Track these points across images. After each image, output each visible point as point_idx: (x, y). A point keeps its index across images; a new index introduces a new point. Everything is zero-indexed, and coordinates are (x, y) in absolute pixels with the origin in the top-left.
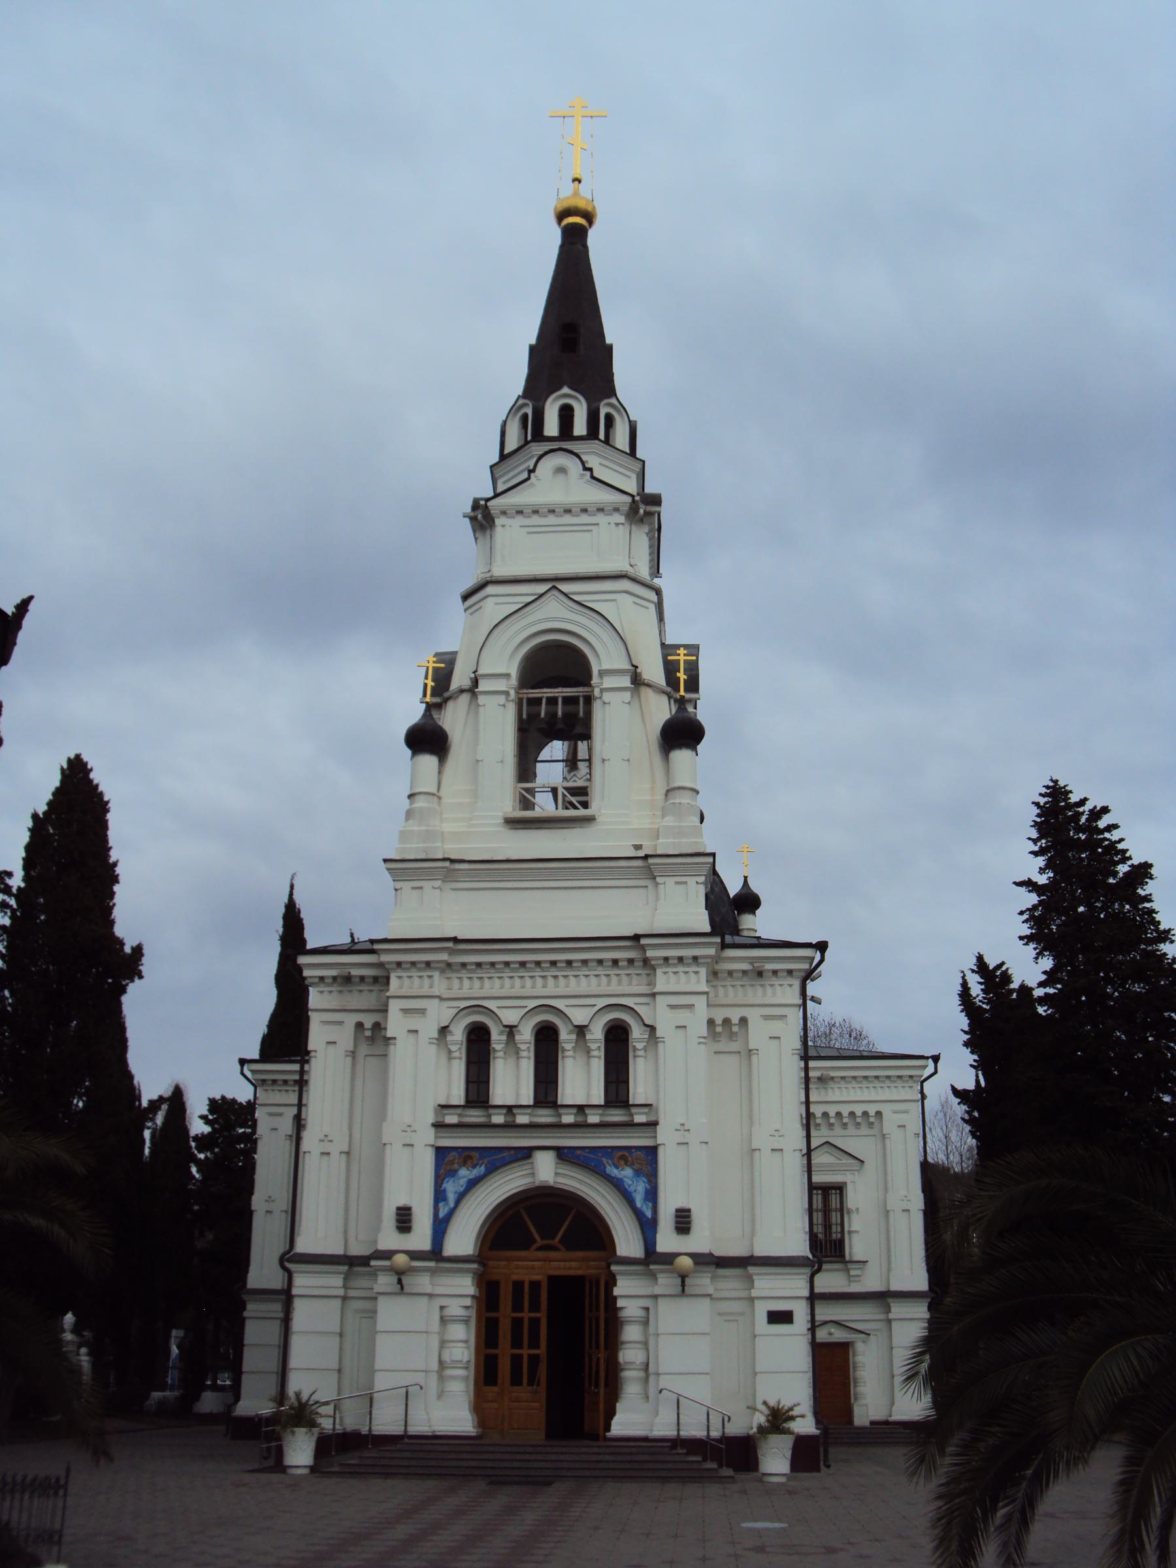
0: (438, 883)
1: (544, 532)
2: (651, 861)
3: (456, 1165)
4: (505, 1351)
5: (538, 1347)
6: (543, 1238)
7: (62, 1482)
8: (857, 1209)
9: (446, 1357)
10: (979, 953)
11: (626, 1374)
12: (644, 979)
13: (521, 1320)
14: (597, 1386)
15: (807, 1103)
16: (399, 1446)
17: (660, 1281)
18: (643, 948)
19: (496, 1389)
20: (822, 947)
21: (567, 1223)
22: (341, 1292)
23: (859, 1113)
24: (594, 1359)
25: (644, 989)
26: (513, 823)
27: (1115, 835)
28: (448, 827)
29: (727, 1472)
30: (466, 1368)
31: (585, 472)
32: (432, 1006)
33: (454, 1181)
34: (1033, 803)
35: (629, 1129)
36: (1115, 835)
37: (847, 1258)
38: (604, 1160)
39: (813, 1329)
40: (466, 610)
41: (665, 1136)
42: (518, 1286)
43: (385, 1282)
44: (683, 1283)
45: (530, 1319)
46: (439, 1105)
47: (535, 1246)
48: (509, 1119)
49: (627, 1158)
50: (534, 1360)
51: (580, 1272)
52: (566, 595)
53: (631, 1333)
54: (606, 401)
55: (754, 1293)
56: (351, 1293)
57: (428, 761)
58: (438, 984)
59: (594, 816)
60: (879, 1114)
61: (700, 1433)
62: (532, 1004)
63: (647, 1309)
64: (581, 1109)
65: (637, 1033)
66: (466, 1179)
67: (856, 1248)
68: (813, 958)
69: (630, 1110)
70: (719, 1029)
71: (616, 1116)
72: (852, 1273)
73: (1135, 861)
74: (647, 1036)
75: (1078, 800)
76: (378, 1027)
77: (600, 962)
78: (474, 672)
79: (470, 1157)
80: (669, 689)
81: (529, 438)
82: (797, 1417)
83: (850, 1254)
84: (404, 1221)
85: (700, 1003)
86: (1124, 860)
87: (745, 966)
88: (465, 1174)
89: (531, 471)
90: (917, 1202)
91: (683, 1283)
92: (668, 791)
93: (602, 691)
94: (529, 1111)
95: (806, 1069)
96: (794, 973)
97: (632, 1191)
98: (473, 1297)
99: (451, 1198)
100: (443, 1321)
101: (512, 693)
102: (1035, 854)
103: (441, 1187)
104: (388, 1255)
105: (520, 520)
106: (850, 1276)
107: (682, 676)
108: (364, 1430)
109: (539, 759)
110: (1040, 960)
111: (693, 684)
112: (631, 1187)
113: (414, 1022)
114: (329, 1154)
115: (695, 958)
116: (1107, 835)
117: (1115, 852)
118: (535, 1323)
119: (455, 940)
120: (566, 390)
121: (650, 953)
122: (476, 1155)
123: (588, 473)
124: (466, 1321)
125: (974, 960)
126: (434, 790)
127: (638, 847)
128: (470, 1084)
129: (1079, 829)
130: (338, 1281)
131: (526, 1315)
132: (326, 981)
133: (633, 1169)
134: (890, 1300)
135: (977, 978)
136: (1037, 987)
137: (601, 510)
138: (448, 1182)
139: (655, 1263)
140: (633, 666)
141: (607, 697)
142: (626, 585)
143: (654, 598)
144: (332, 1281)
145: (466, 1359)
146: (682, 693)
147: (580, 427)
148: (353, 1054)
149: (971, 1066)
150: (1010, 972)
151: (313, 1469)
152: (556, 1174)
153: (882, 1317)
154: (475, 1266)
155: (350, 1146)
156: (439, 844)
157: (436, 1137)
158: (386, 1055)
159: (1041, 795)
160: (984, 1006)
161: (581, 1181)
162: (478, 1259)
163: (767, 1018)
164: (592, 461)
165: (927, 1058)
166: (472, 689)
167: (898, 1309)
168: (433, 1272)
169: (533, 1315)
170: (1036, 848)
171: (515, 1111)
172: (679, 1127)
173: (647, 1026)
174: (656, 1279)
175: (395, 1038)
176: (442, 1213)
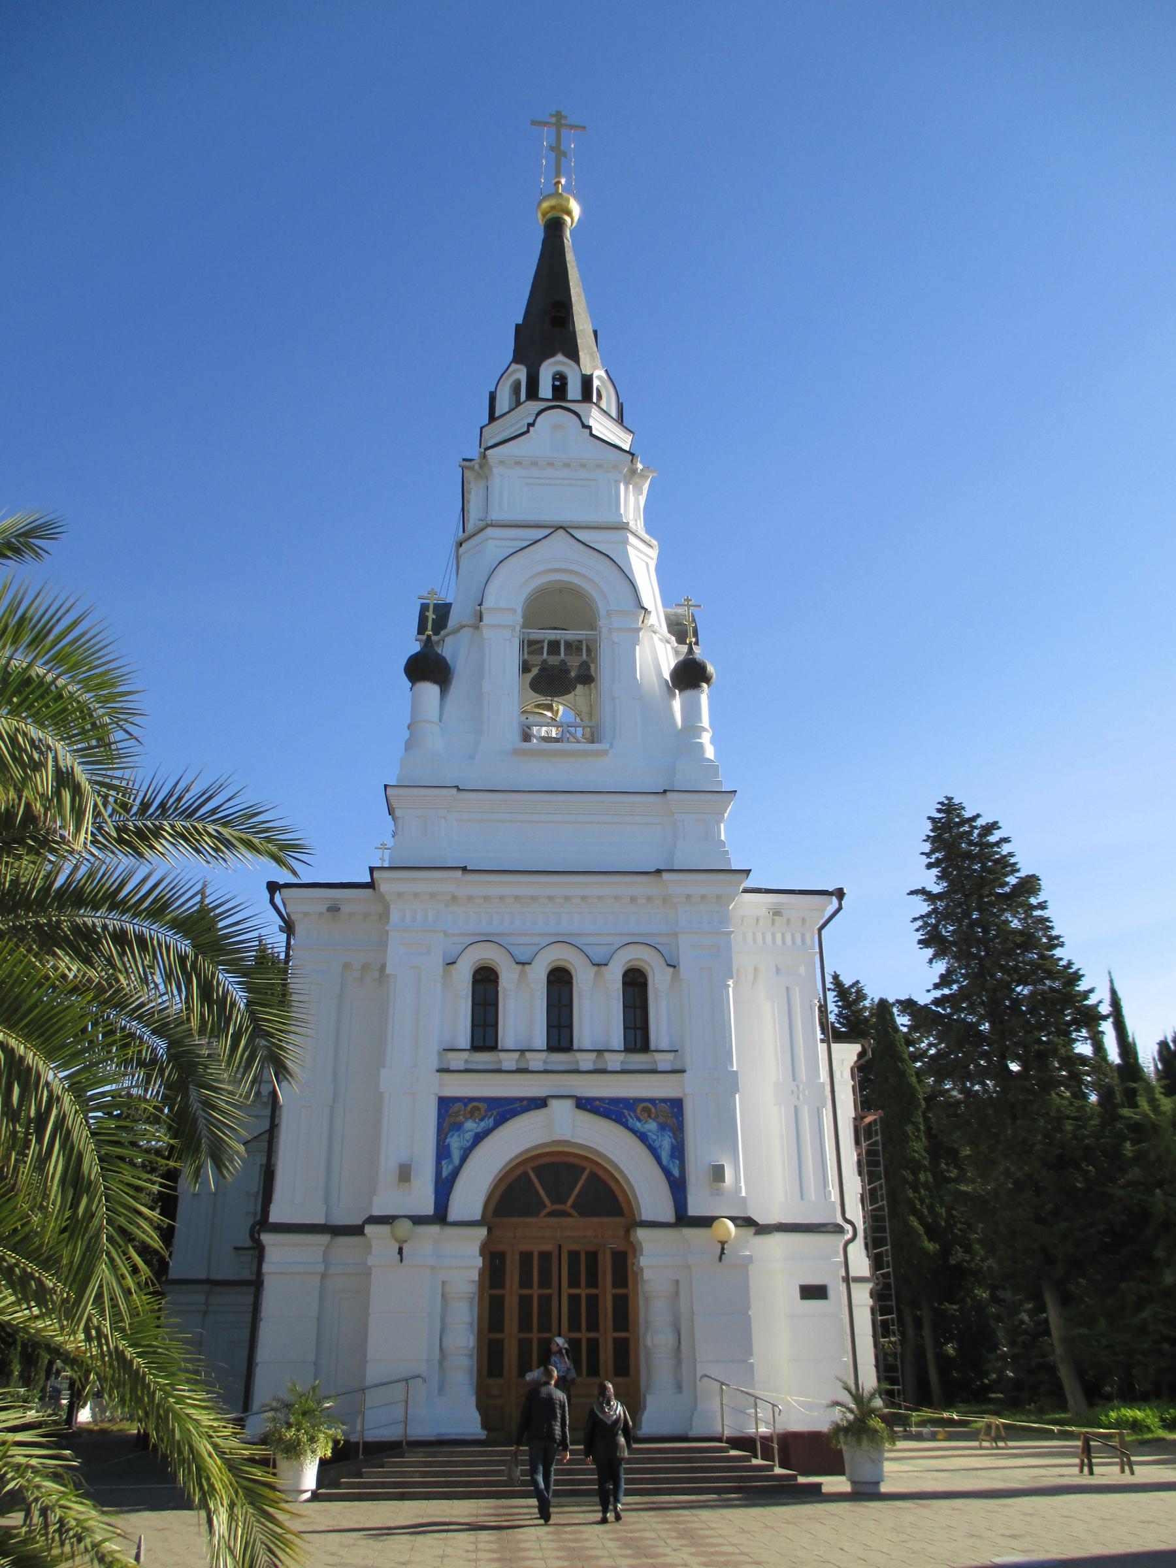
3: (461, 1117)
6: (553, 1202)
10: (835, 972)
27: (1005, 849)
31: (584, 430)
33: (459, 1136)
36: (1005, 849)
42: (526, 1257)
49: (650, 1109)
57: (430, 690)
66: (472, 1134)
73: (1022, 874)
75: (970, 816)
84: (405, 1174)
89: (530, 425)
97: (657, 1146)
99: (456, 1155)
103: (444, 1142)
110: (934, 964)
112: (656, 1143)
117: (1005, 865)
119: (464, 869)
123: (587, 431)
128: (475, 1028)
131: (583, 1291)
133: (657, 1122)
136: (934, 989)
137: (599, 466)
138: (452, 1137)
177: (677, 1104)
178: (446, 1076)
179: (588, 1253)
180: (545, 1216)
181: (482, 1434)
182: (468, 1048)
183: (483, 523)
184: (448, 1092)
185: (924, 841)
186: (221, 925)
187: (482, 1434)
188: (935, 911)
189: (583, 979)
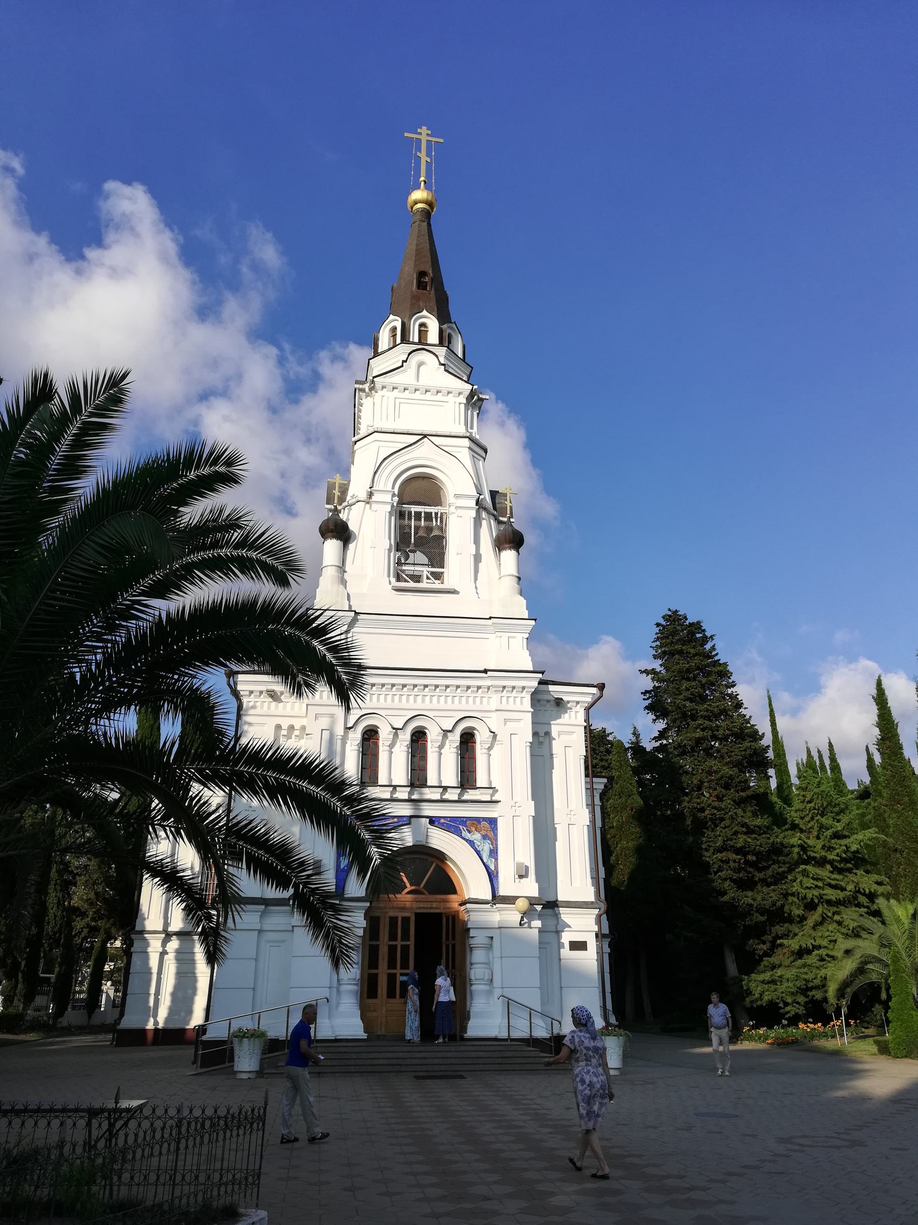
4: (383, 971)
42: (393, 921)
47: (406, 890)
74: (491, 740)
78: (370, 488)
81: (398, 341)
107: (337, 493)
118: (405, 949)
151: (260, 1073)
169: (394, 943)
173: (491, 732)
177: (493, 822)
179: (403, 918)
181: (365, 1036)
183: (371, 430)
184: (385, 992)
185: (654, 721)
186: (215, 717)
187: (365, 1036)
189: (433, 736)
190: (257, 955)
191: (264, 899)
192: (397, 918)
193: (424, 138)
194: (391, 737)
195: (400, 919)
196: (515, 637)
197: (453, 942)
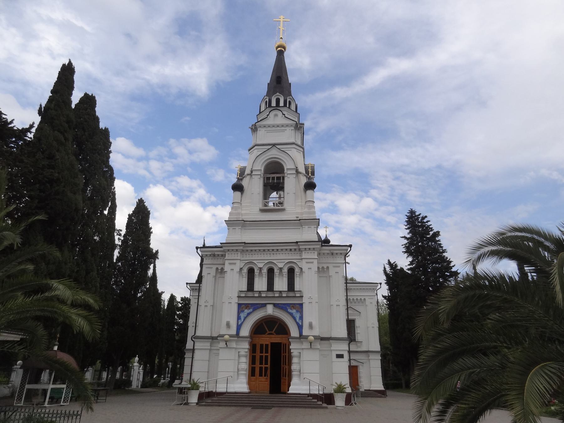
0: (240, 227)
1: (271, 132)
2: (301, 221)
4: (257, 366)
5: (268, 365)
7: (79, 413)
8: (359, 326)
9: (240, 367)
11: (293, 373)
12: (298, 255)
13: (262, 356)
14: (285, 376)
15: (347, 296)
16: (224, 396)
17: (304, 344)
18: (299, 246)
19: (255, 377)
20: (350, 246)
21: (276, 327)
22: (209, 348)
23: (359, 299)
24: (285, 368)
25: (299, 257)
26: (262, 211)
27: (429, 223)
28: (243, 212)
29: (325, 405)
30: (246, 371)
32: (238, 262)
34: (406, 215)
35: (295, 298)
36: (429, 223)
37: (356, 341)
38: (287, 307)
39: (350, 360)
40: (249, 154)
41: (305, 300)
42: (262, 346)
43: (222, 344)
44: (311, 344)
45: (265, 356)
46: (239, 291)
47: (267, 334)
48: (260, 295)
50: (266, 368)
51: (280, 341)
52: (278, 149)
53: (295, 360)
54: (289, 97)
55: (332, 348)
56: (213, 348)
57: (238, 194)
58: (239, 256)
59: (285, 208)
60: (365, 299)
61: (317, 392)
62: (267, 261)
63: (300, 353)
64: (281, 292)
65: (297, 270)
66: (247, 313)
67: (359, 337)
68: (348, 249)
69: (295, 292)
70: (321, 270)
71: (291, 294)
72: (358, 345)
73: (435, 231)
75: (418, 214)
76: (222, 269)
77: (286, 250)
79: (248, 306)
80: (306, 175)
81: (268, 107)
82: (347, 388)
83: (357, 340)
84: (228, 325)
85: (316, 262)
86: (432, 230)
87: (328, 252)
88: (247, 311)
90: (377, 324)
91: (311, 344)
92: (306, 202)
93: (288, 174)
94: (265, 292)
95: (346, 286)
96: (342, 254)
98: (248, 349)
100: (239, 356)
101: (262, 175)
102: (406, 229)
104: (222, 336)
105: (265, 129)
106: (357, 346)
107: (310, 170)
108: (214, 391)
109: (270, 197)
111: (313, 173)
113: (232, 267)
114: (207, 306)
115: (314, 249)
116: (427, 224)
117: (429, 229)
118: (266, 357)
119: (245, 243)
120: (278, 94)
121: (301, 247)
122: (250, 306)
123: (284, 116)
124: (246, 356)
125: (387, 261)
126: (240, 202)
127: (297, 217)
129: (419, 222)
130: (209, 344)
131: (264, 354)
132: (208, 256)
134: (369, 353)
135: (388, 266)
137: (287, 126)
139: (302, 338)
140: (296, 167)
141: (288, 176)
142: (294, 146)
143: (302, 150)
144: (206, 344)
145: (246, 368)
146: (310, 175)
147: (282, 104)
148: (215, 277)
149: (387, 289)
150: (397, 264)
152: (273, 311)
153: (367, 358)
154: (249, 339)
155: (214, 303)
156: (241, 216)
157: (238, 300)
158: (224, 277)
159: (408, 213)
160: (390, 273)
161: (279, 313)
162: (250, 337)
163: (334, 267)
164: (284, 113)
165: (378, 283)
166: (251, 174)
167: (372, 356)
168: (237, 341)
170: (407, 227)
171: (261, 292)
172: (309, 298)
173: (300, 268)
174: (303, 343)
175: (227, 271)
176: (239, 323)
178: (239, 298)
179: (266, 345)
180: (267, 334)
182: (246, 290)
184: (258, 375)
188: (408, 242)
190: (209, 359)
191: (212, 337)
192: (263, 345)
193: (282, 20)
194: (259, 271)
195: (264, 345)
196: (311, 227)
197: (285, 354)
